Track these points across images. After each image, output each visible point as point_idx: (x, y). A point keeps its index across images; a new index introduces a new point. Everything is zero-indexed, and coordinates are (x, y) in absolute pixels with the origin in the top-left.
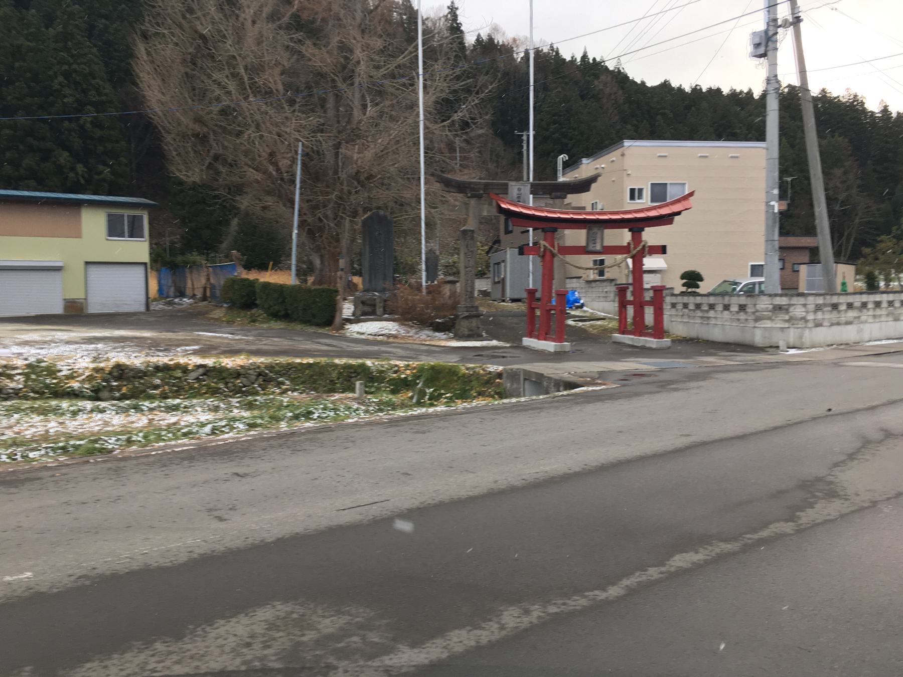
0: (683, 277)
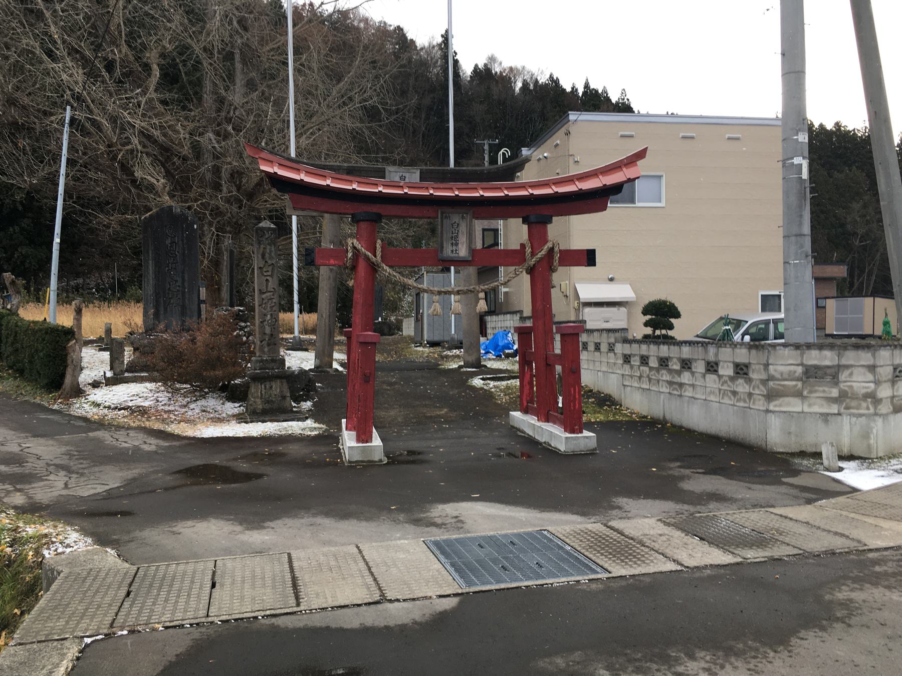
0: (645, 312)
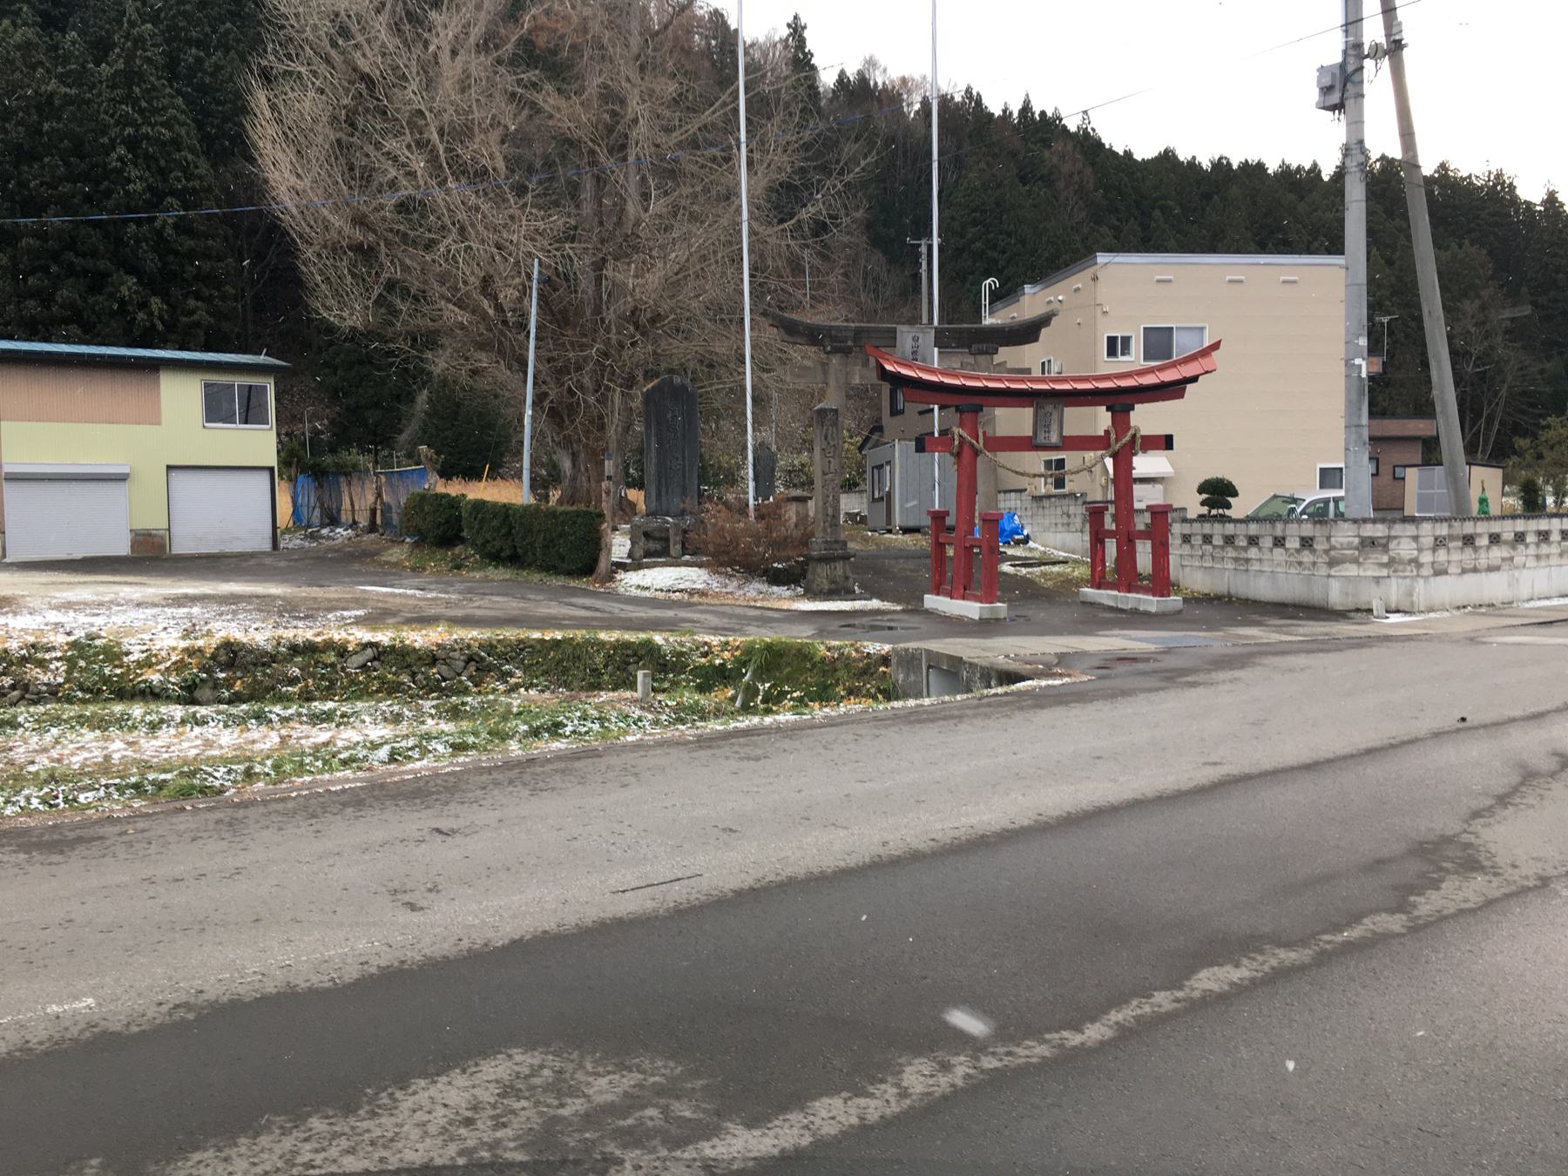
0: (1201, 490)
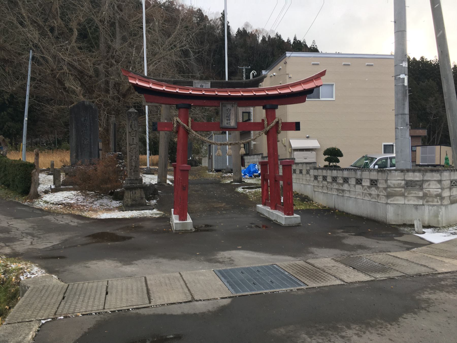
0: (325, 154)
